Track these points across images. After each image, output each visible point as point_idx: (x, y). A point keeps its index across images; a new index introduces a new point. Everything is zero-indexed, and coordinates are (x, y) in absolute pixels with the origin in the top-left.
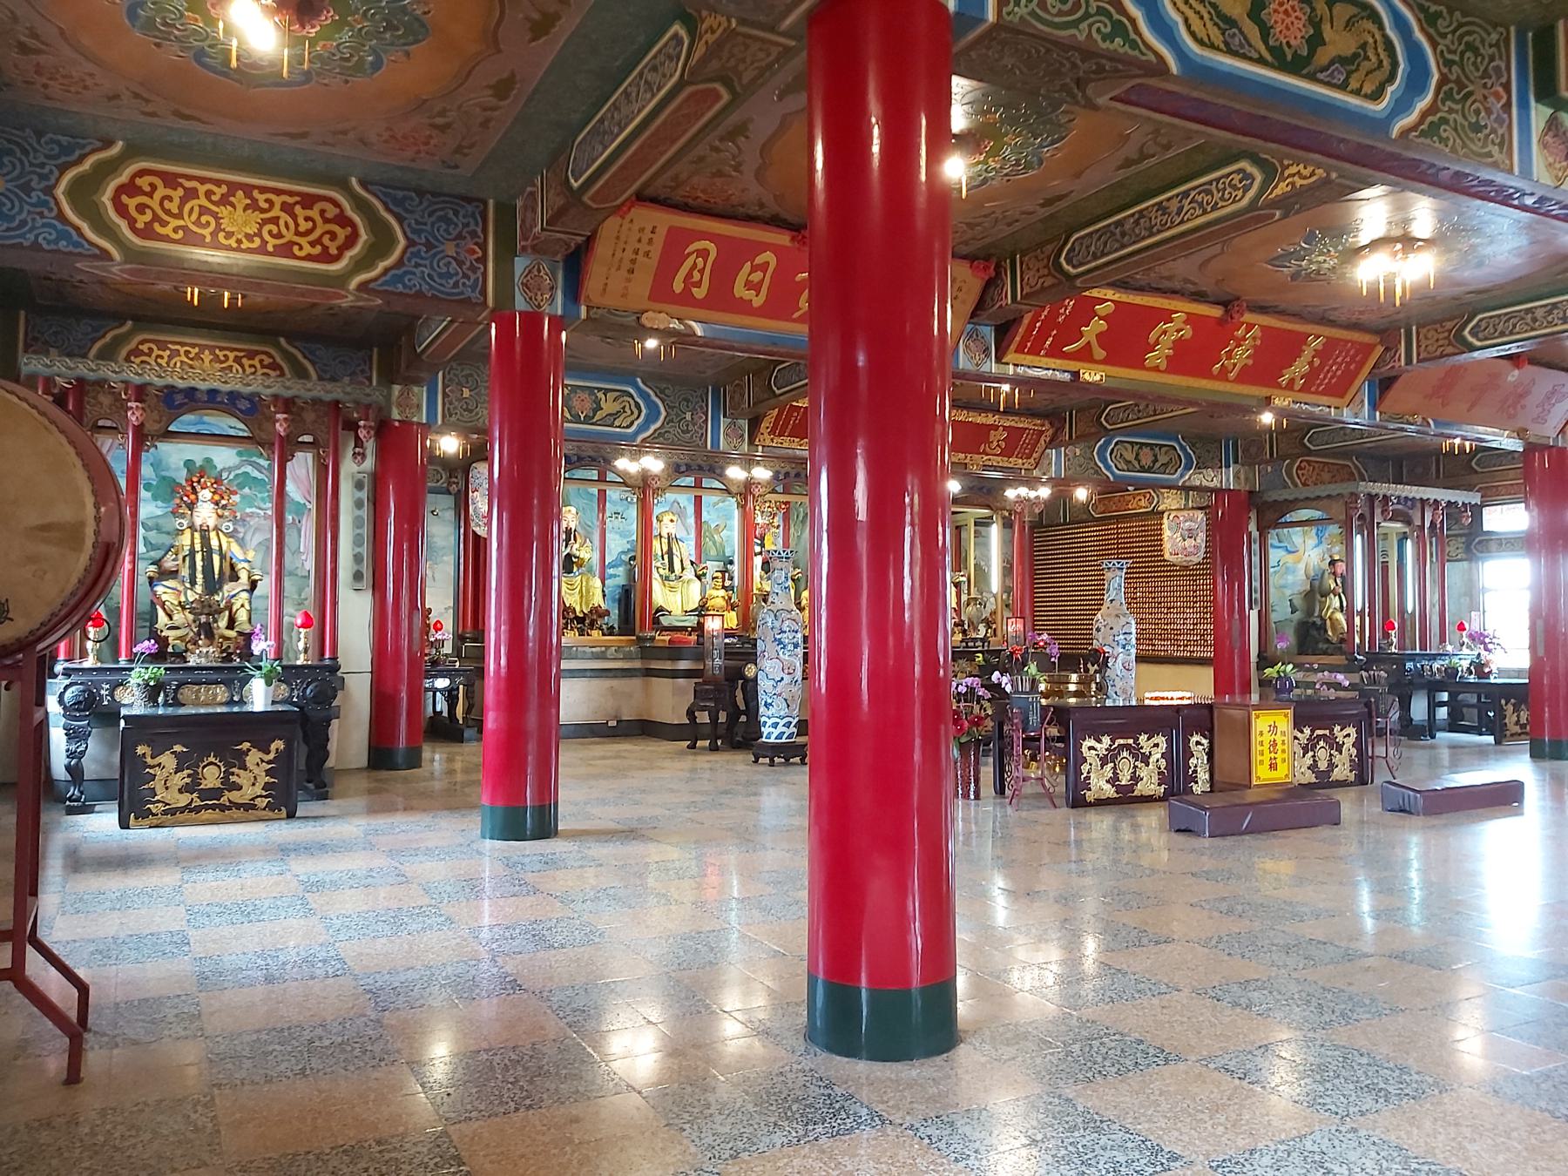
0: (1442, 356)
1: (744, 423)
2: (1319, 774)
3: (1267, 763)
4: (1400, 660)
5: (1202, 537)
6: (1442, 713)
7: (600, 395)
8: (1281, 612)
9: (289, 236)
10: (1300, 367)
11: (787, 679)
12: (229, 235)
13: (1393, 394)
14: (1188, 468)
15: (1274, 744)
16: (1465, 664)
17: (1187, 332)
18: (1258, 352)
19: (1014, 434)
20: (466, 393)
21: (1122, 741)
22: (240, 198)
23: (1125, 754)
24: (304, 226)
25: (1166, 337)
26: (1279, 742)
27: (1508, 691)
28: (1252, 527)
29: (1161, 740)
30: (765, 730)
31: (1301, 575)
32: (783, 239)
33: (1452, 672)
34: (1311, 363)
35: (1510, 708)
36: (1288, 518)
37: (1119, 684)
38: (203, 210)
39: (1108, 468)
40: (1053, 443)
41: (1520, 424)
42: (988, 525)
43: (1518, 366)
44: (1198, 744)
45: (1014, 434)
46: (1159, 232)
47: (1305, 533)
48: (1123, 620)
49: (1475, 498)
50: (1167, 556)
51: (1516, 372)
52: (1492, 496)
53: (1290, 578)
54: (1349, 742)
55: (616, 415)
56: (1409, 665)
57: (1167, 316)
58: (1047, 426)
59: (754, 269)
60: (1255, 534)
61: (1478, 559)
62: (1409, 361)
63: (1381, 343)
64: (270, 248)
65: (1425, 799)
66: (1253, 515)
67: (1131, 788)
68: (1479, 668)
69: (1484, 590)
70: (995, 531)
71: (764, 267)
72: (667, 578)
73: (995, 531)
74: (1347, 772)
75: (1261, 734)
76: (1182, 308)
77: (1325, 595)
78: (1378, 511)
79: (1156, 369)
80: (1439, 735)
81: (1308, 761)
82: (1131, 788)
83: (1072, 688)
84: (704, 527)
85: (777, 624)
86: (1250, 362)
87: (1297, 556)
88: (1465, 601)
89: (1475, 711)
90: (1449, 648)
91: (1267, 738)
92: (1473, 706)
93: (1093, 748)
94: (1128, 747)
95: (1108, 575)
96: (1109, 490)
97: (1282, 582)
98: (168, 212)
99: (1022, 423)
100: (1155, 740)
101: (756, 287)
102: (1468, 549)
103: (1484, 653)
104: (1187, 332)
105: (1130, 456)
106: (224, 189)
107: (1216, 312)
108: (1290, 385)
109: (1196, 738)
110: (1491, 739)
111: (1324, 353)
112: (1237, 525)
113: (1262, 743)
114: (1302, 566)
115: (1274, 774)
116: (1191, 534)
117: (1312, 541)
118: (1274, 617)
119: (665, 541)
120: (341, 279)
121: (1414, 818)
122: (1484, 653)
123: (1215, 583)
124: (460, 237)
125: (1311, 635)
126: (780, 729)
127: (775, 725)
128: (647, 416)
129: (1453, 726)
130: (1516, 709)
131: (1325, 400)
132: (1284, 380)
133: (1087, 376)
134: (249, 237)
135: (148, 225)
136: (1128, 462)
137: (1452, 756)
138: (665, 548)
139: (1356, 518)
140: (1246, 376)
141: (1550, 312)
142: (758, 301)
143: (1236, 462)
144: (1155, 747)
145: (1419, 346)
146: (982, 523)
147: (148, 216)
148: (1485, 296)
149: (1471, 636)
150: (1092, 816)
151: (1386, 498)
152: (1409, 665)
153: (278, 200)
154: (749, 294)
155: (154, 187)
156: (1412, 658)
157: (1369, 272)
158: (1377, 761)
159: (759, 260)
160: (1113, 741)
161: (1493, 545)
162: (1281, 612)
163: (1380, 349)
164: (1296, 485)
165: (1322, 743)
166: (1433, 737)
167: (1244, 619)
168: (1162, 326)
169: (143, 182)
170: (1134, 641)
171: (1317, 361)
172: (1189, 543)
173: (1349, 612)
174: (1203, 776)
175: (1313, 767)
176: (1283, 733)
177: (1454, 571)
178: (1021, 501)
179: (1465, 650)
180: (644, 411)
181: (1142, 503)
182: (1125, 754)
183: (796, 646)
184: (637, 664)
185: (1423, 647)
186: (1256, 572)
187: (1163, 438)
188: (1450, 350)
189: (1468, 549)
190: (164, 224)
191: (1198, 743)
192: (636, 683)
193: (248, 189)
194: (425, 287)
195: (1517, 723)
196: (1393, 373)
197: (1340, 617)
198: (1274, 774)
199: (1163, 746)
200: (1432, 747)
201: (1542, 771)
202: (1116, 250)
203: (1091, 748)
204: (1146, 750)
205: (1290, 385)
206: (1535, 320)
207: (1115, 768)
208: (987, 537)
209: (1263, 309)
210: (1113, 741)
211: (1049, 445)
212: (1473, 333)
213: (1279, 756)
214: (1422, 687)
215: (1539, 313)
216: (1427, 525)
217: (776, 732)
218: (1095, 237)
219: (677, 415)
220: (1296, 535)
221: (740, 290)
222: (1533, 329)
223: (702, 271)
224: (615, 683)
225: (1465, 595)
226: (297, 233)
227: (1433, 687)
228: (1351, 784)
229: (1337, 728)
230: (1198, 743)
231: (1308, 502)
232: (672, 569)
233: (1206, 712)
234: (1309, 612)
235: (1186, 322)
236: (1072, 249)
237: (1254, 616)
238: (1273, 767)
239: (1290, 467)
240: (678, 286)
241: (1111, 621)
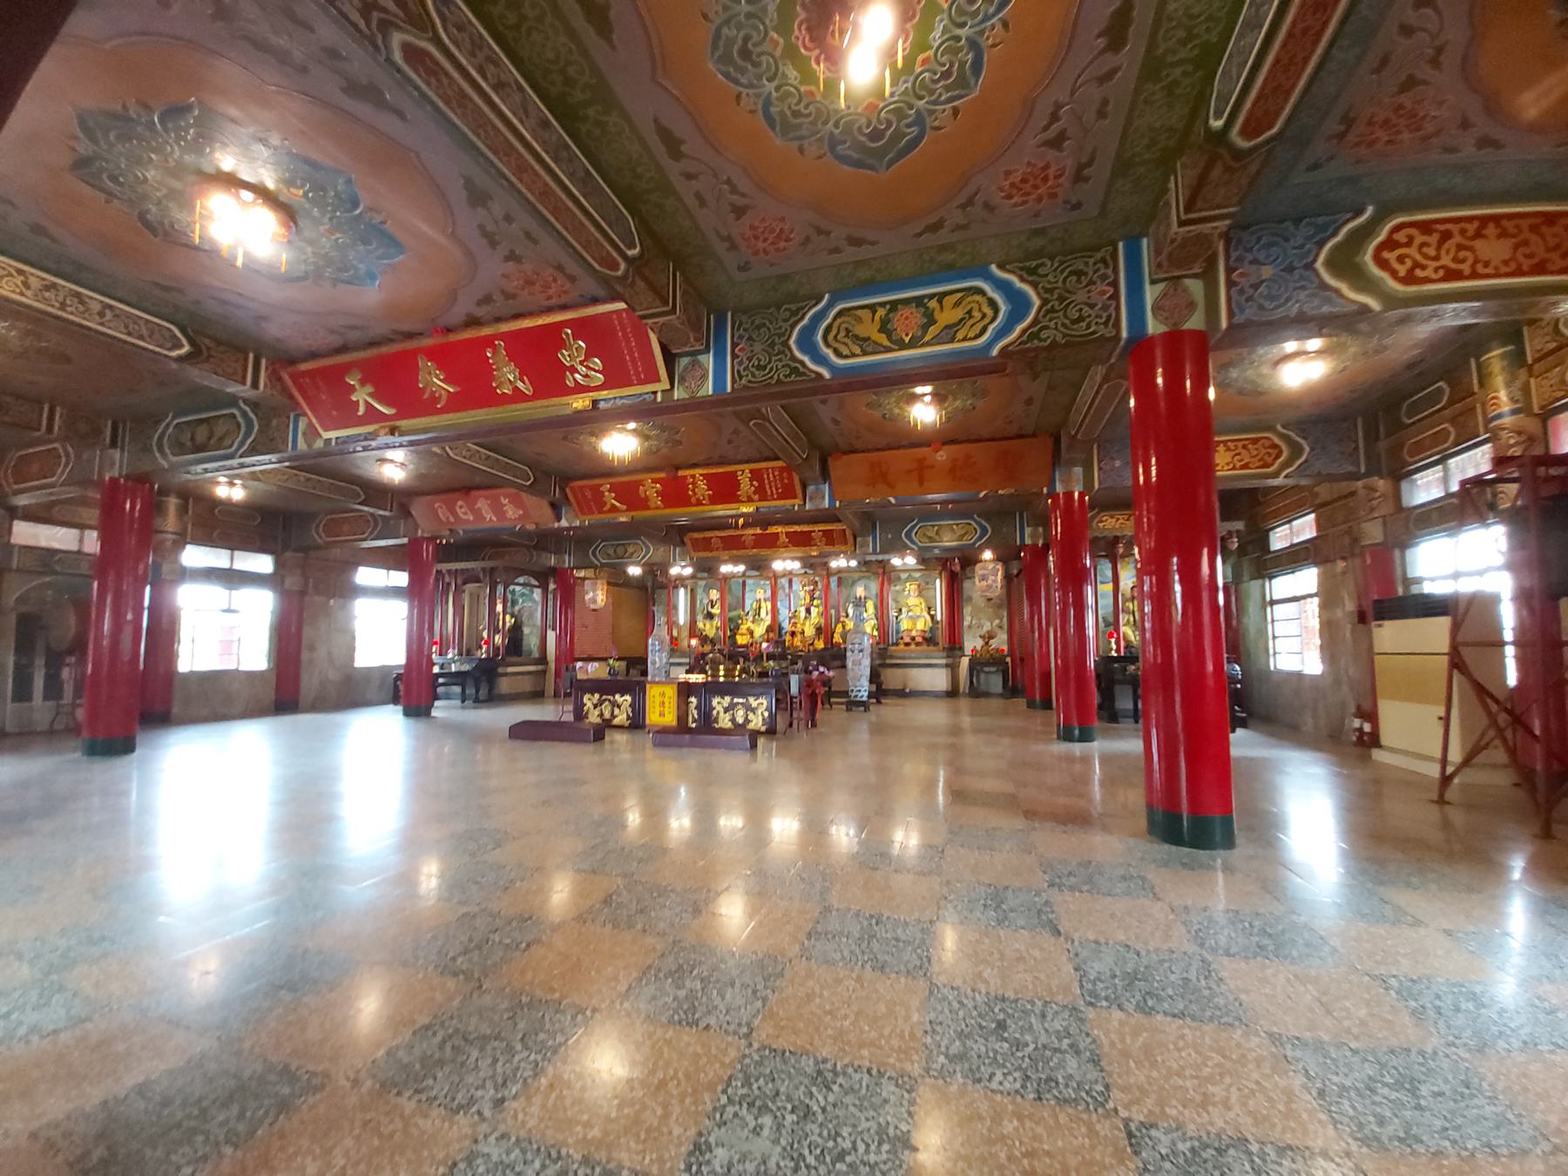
9: (1541, 253)
12: (1486, 264)
22: (1491, 230)
24: (1552, 242)
29: (628, 698)
38: (1460, 247)
64: (1525, 268)
81: (597, 712)
91: (658, 700)
93: (589, 700)
98: (1426, 256)
106: (1476, 224)
120: (174, 418)
124: (1092, 282)
134: (1506, 263)
135: (1411, 271)
147: (1409, 263)
153: (1525, 223)
155: (1411, 239)
169: (1401, 237)
175: (601, 715)
190: (1423, 267)
193: (1496, 219)
194: (1059, 337)
219: (1061, 299)
226: (1549, 250)
238: (662, 714)
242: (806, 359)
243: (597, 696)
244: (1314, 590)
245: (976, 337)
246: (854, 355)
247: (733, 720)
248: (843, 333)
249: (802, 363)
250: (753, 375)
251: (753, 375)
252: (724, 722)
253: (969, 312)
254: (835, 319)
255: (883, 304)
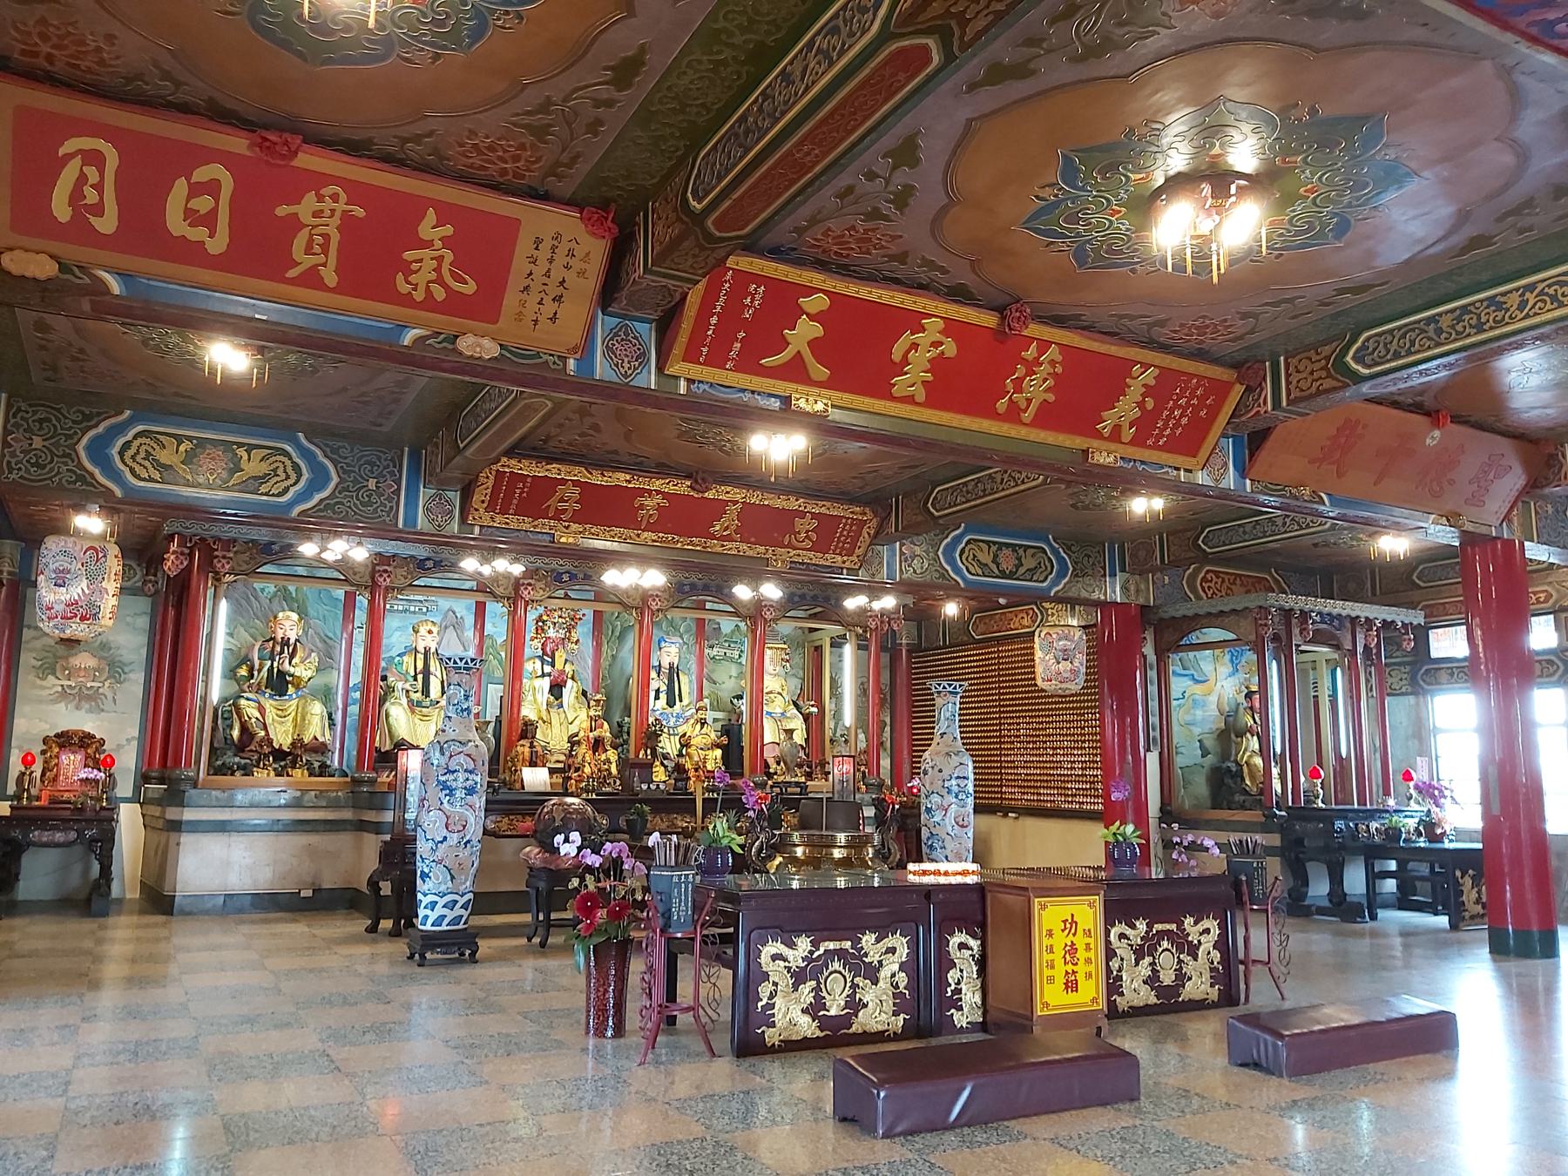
0: (1319, 393)
1: (455, 497)
2: (1161, 991)
3: (1060, 980)
4: (1327, 817)
5: (1080, 661)
6: (1390, 885)
7: (242, 452)
8: (1188, 755)
10: (1126, 409)
11: (454, 839)
13: (1264, 455)
14: (1062, 574)
15: (1072, 950)
16: (1412, 823)
17: (950, 348)
18: (1060, 383)
19: (827, 525)
20: (38, 442)
21: (831, 945)
23: (836, 965)
25: (921, 351)
26: (1080, 946)
27: (1464, 859)
28: (1149, 650)
29: (900, 942)
30: (422, 912)
31: (1212, 710)
32: (238, 144)
33: (1393, 834)
34: (1141, 405)
35: (1468, 881)
36: (1194, 638)
37: (950, 845)
39: (957, 571)
40: (878, 537)
41: (1449, 507)
42: (840, 646)
43: (1436, 424)
44: (962, 946)
45: (827, 525)
46: (784, 113)
47: (1216, 659)
48: (955, 760)
49: (1418, 618)
50: (1039, 682)
51: (1437, 433)
52: (1438, 617)
53: (1199, 713)
54: (1208, 942)
55: (263, 479)
56: (1339, 824)
57: (914, 321)
58: (869, 515)
59: (196, 190)
60: (1152, 658)
61: (1425, 693)
62: (1277, 403)
63: (1240, 380)
65: (1289, 1047)
66: (1149, 635)
67: (846, 1021)
68: (1429, 827)
69: (1436, 730)
70: (848, 650)
71: (212, 188)
72: (419, 704)
73: (848, 650)
74: (1206, 987)
75: (1050, 934)
76: (938, 310)
77: (1240, 735)
78: (1296, 631)
79: (909, 400)
80: (1381, 913)
81: (1144, 969)
82: (846, 1021)
83: (837, 854)
84: (488, 642)
85: (443, 761)
86: (1051, 397)
87: (1208, 686)
88: (1413, 744)
89: (1428, 885)
90: (1391, 802)
91: (1060, 940)
92: (1422, 879)
93: (779, 957)
94: (841, 954)
95: (939, 701)
96: (982, 602)
97: (1188, 718)
99: (837, 510)
100: (889, 942)
101: (209, 221)
102: (1413, 681)
103: (1434, 809)
104: (950, 348)
105: (986, 558)
107: (989, 320)
108: (1115, 435)
109: (956, 940)
110: (1443, 921)
111: (1161, 390)
112: (1130, 648)
113: (1051, 950)
114: (1213, 699)
115: (1072, 998)
116: (1066, 656)
117: (1224, 669)
118: (1180, 761)
119: (420, 657)
121: (1274, 1080)
122: (1434, 809)
123: (1102, 720)
125: (1226, 782)
126: (439, 911)
127: (433, 905)
128: (311, 482)
129: (1404, 902)
130: (1476, 882)
131: (1165, 457)
132: (1106, 427)
133: (802, 403)
136: (983, 565)
137: (1406, 946)
138: (420, 665)
139: (1273, 638)
140: (1047, 417)
141: (1459, 320)
142: (217, 244)
143: (1123, 570)
144: (890, 954)
145: (1288, 383)
146: (837, 643)
148: (1365, 297)
149: (1417, 787)
150: (773, 1069)
151: (1305, 615)
152: (1339, 824)
154: (199, 234)
156: (1343, 815)
157: (1174, 229)
158: (1254, 969)
159: (202, 174)
160: (816, 945)
161: (1444, 676)
162: (1188, 755)
163: (1239, 389)
164: (1199, 598)
165: (1165, 944)
166: (1373, 917)
167: (1139, 765)
168: (906, 339)
170: (971, 788)
171: (1150, 403)
172: (1065, 666)
173: (1265, 751)
174: (971, 996)
175: (1152, 980)
176: (1087, 933)
177: (1398, 708)
178: (863, 612)
179: (1414, 806)
180: (306, 475)
181: (1025, 622)
182: (836, 965)
183: (470, 791)
184: (347, 814)
185: (1362, 801)
186: (1154, 705)
187: (1028, 539)
188: (1329, 383)
189: (1413, 681)
191: (962, 946)
192: (344, 840)
195: (1478, 901)
196: (1260, 425)
197: (1258, 761)
198: (1072, 998)
199: (903, 952)
200: (1374, 934)
201: (1504, 977)
202: (741, 158)
203: (775, 957)
204: (873, 958)
205: (1115, 435)
206: (1439, 331)
207: (817, 990)
208: (841, 655)
209: (1059, 321)
210: (816, 945)
211: (876, 538)
212: (1358, 359)
213: (1081, 969)
214: (1355, 852)
215: (1445, 323)
216: (1360, 649)
217: (433, 916)
218: (720, 148)
219: (355, 481)
220: (1205, 659)
221: (176, 223)
222: (1438, 345)
223: (99, 187)
224: (313, 839)
225: (1414, 736)
227: (1372, 853)
228: (1214, 1005)
229: (1189, 921)
230: (962, 946)
231: (1215, 619)
232: (426, 691)
233: (975, 897)
234: (1225, 755)
235: (945, 332)
236: (1364, 347)
237: (1152, 761)
239: (1193, 576)
240: (61, 209)
241: (939, 761)
242: (97, 472)
243: (804, 944)
244: (1562, 721)
245: (280, 495)
246: (151, 480)
247: (815, 1009)
248: (143, 455)
249: (92, 475)
250: (27, 471)
251: (27, 471)
252: (790, 1015)
253: (275, 470)
254: (135, 437)
255: (190, 439)
